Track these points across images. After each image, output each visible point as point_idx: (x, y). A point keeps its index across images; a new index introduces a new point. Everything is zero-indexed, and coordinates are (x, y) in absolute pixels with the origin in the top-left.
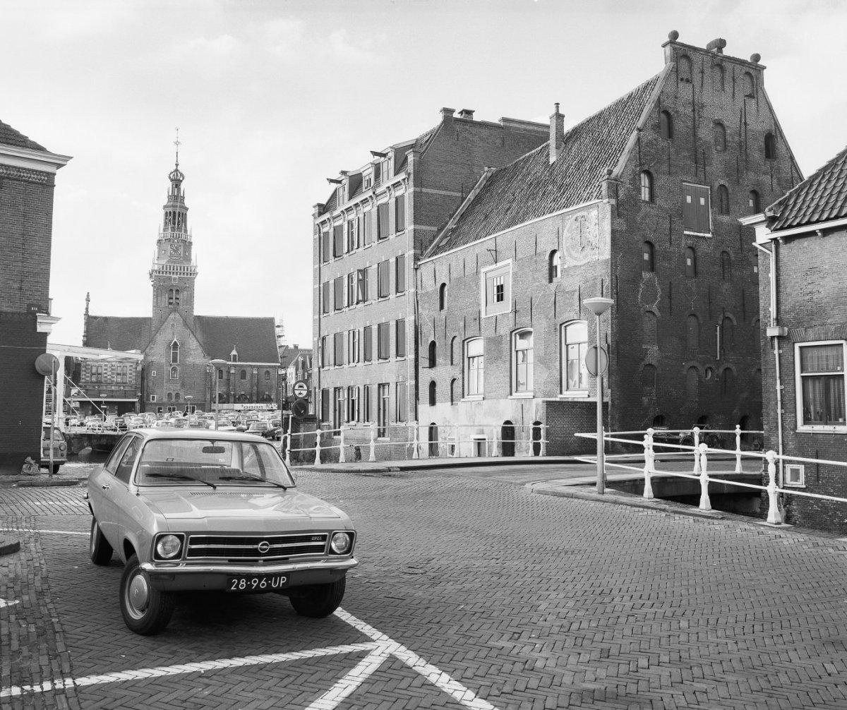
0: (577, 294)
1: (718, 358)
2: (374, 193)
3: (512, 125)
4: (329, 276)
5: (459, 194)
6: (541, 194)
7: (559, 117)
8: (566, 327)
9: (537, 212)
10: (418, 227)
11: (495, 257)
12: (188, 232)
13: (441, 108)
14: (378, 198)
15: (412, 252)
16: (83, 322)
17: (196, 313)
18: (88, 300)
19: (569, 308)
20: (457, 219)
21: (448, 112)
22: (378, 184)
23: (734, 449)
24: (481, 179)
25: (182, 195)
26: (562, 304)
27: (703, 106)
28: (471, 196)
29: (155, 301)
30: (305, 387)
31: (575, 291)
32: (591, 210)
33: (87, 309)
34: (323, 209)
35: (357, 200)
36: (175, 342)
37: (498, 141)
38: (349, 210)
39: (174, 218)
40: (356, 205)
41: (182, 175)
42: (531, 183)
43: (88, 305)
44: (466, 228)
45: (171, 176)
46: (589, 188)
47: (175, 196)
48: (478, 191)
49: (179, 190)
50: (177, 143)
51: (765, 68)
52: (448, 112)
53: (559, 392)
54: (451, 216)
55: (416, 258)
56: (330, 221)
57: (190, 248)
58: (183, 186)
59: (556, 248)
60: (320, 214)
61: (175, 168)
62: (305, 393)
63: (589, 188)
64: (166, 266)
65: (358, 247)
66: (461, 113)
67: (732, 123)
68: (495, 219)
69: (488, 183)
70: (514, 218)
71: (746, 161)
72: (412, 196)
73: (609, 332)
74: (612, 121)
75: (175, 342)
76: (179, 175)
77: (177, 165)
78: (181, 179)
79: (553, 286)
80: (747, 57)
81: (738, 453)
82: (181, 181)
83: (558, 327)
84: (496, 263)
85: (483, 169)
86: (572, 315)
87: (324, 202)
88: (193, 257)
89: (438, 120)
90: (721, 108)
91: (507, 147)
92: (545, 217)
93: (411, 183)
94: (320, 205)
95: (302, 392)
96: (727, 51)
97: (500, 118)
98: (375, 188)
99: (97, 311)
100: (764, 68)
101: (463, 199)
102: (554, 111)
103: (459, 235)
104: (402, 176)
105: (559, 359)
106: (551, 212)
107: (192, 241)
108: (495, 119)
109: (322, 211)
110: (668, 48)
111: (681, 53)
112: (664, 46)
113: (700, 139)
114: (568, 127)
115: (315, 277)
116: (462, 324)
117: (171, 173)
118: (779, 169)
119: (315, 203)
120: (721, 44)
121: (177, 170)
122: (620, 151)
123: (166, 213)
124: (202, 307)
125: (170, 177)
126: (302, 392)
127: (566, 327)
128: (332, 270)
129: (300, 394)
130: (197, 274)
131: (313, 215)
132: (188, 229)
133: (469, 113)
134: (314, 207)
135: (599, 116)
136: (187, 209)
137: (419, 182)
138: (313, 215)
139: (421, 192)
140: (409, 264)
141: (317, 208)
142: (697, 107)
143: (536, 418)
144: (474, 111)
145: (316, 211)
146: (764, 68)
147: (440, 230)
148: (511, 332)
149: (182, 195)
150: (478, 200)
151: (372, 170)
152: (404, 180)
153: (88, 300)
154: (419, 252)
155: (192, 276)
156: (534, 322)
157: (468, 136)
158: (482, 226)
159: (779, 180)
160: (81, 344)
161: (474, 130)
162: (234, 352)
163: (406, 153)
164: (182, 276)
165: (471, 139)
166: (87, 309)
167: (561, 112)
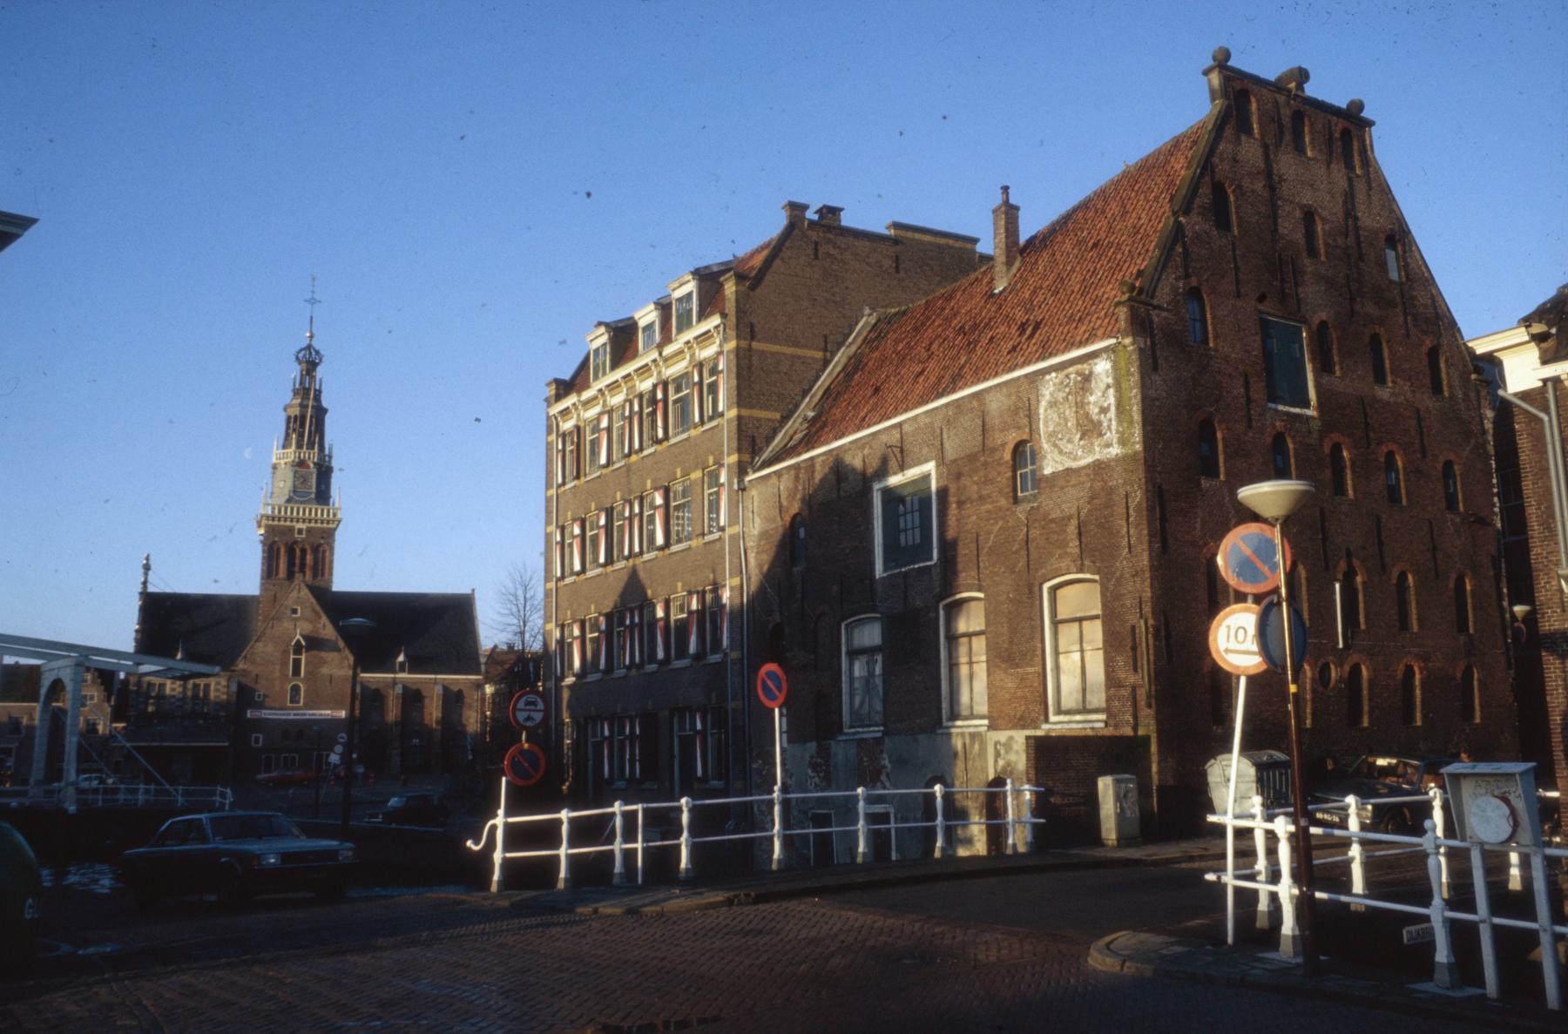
3: (910, 234)
5: (819, 355)
7: (1009, 213)
8: (1054, 589)
10: (746, 412)
11: (900, 459)
13: (785, 202)
16: (136, 603)
18: (147, 568)
20: (818, 397)
21: (796, 209)
23: (571, 845)
27: (1281, 179)
30: (541, 706)
31: (1070, 518)
32: (1096, 361)
35: (629, 368)
36: (298, 641)
37: (888, 263)
38: (613, 386)
40: (627, 377)
41: (317, 352)
43: (146, 574)
44: (837, 412)
45: (301, 355)
47: (304, 389)
48: (853, 348)
49: (313, 378)
50: (313, 301)
52: (796, 209)
53: (1042, 718)
54: (805, 393)
55: (741, 470)
56: (576, 409)
58: (320, 372)
59: (1025, 437)
60: (559, 397)
61: (308, 341)
62: (538, 717)
69: (873, 335)
75: (298, 641)
76: (313, 353)
80: (1342, 103)
81: (618, 846)
82: (317, 364)
89: (773, 225)
94: (558, 382)
96: (1311, 90)
97: (889, 221)
98: (660, 347)
99: (168, 582)
100: (1370, 124)
101: (826, 363)
102: (998, 199)
108: (879, 226)
112: (1206, 73)
114: (1028, 228)
119: (551, 378)
125: (297, 358)
126: (533, 714)
129: (529, 718)
130: (339, 521)
134: (548, 384)
135: (1084, 206)
139: (750, 349)
141: (554, 386)
144: (841, 210)
145: (552, 391)
147: (785, 419)
153: (147, 568)
154: (746, 457)
155: (331, 526)
157: (832, 251)
158: (868, 407)
161: (840, 241)
162: (401, 658)
164: (312, 525)
165: (839, 257)
166: (145, 583)
167: (1012, 201)
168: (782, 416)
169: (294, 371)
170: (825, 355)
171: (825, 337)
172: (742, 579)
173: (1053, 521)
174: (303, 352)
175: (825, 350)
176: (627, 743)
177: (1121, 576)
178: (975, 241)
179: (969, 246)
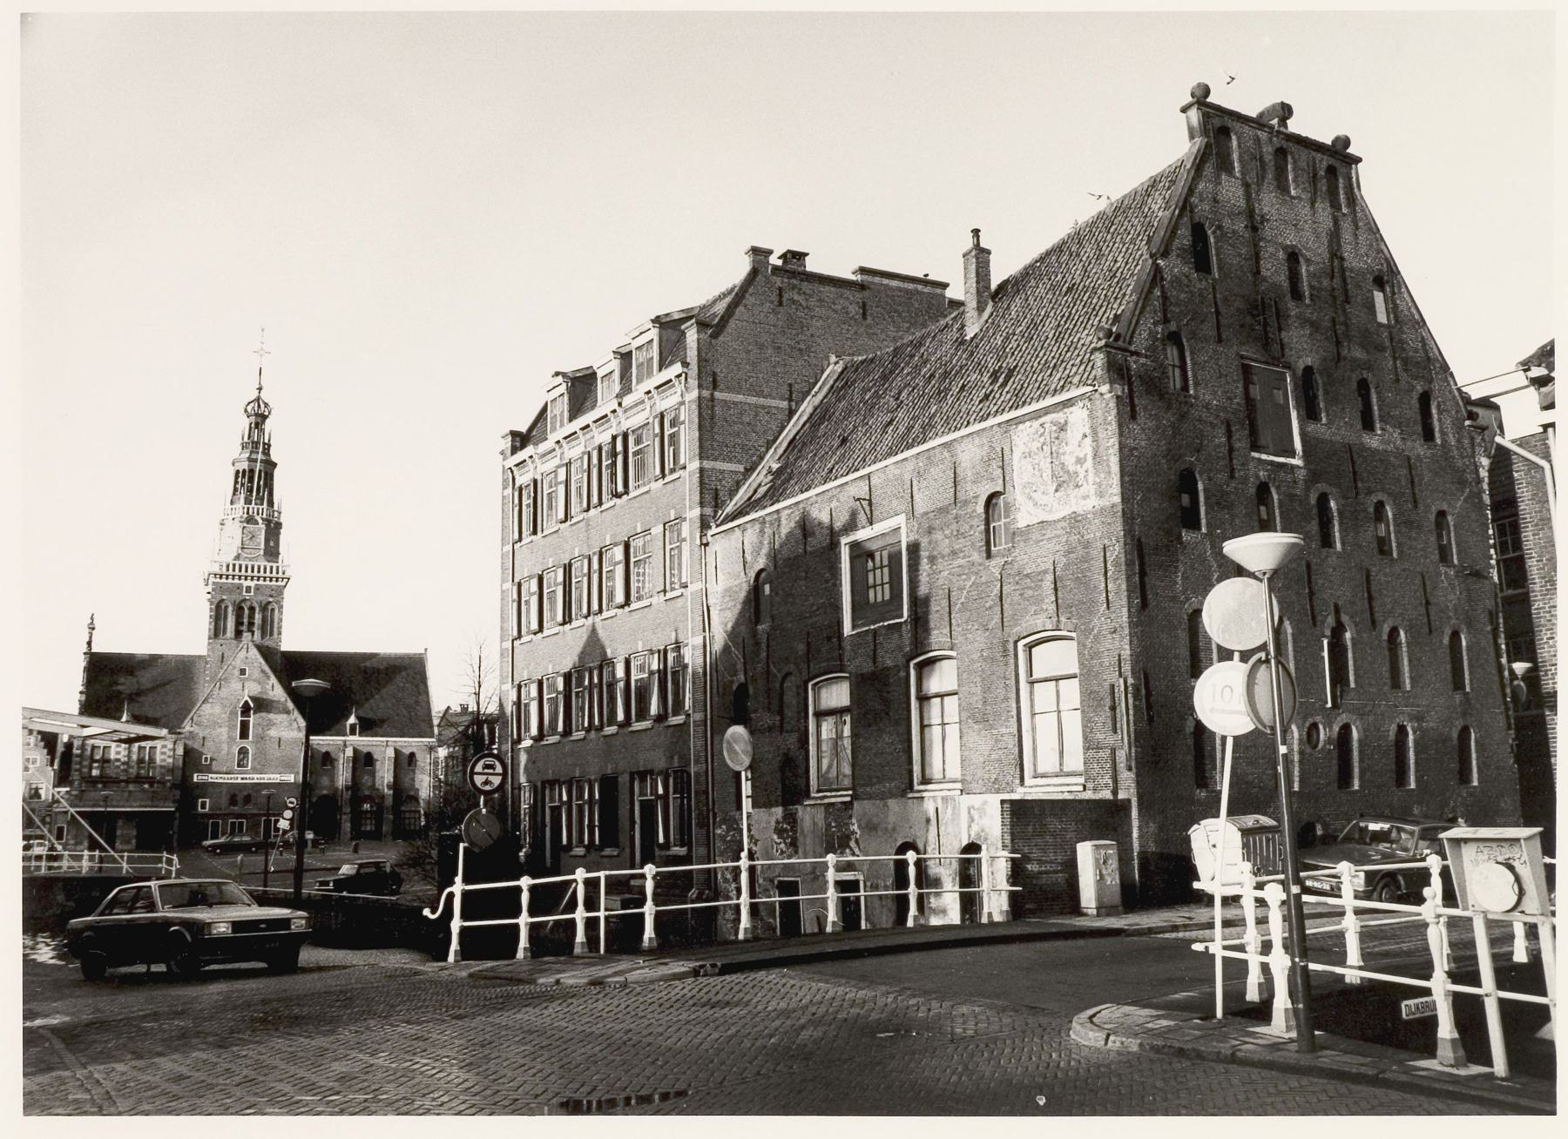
0: (1050, 577)
1: (1329, 705)
2: (620, 404)
4: (527, 567)
5: (784, 404)
6: (955, 390)
7: (980, 256)
9: (950, 425)
10: (708, 464)
12: (276, 508)
13: (749, 247)
14: (629, 413)
15: (697, 512)
16: (81, 663)
17: (283, 649)
19: (1034, 608)
21: (759, 254)
22: (626, 389)
24: (825, 376)
25: (266, 441)
26: (1017, 598)
27: (1263, 219)
28: (806, 408)
29: (212, 627)
30: (499, 769)
31: (1045, 572)
33: (89, 643)
34: (521, 440)
35: (587, 418)
39: (251, 480)
41: (266, 405)
42: (931, 375)
43: (91, 634)
45: (249, 408)
46: (1061, 369)
47: (253, 442)
51: (1358, 160)
52: (759, 254)
54: (769, 445)
55: (704, 525)
57: (279, 534)
58: (269, 425)
59: (999, 489)
60: (514, 450)
63: (1061, 369)
64: (234, 565)
65: (567, 619)
66: (783, 256)
67: (1315, 249)
68: (862, 442)
70: (903, 437)
71: (1346, 325)
72: (694, 407)
73: (1126, 653)
74: (1089, 250)
75: (246, 702)
76: (262, 406)
77: (260, 389)
78: (266, 413)
79: (995, 565)
82: (266, 417)
83: (1011, 647)
84: (871, 524)
85: (827, 358)
86: (1041, 621)
87: (523, 429)
88: (282, 549)
89: (743, 267)
90: (1295, 225)
91: (869, 320)
92: (971, 429)
93: (693, 382)
94: (514, 434)
95: (491, 778)
96: (1295, 126)
101: (791, 413)
102: (969, 243)
103: (791, 478)
104: (677, 368)
105: (1014, 713)
106: (983, 419)
107: (282, 520)
109: (518, 444)
110: (1194, 115)
111: (1217, 122)
112: (1184, 110)
113: (1265, 279)
115: (503, 569)
116: (802, 647)
117: (249, 403)
118: (1402, 342)
120: (1285, 111)
121: (258, 399)
122: (1116, 298)
123: (238, 472)
124: (295, 637)
125: (246, 411)
126: (491, 778)
127: (1030, 647)
128: (539, 555)
129: (486, 783)
131: (502, 453)
132: (275, 501)
133: (799, 256)
136: (275, 465)
137: (709, 378)
138: (502, 453)
140: (689, 530)
142: (1255, 223)
143: (970, 836)
145: (507, 443)
146: (1358, 160)
147: (749, 471)
148: (908, 661)
149: (266, 441)
150: (821, 415)
151: (615, 365)
152: (679, 376)
154: (709, 511)
155: (279, 583)
156: (958, 640)
159: (1405, 361)
160: (76, 712)
161: (805, 286)
163: (683, 327)
164: (261, 582)
165: (804, 303)
166: (89, 643)
168: (745, 469)
169: (245, 423)
170: (790, 406)
171: (790, 385)
172: (705, 637)
173: (1027, 576)
174: (252, 404)
175: (790, 400)
176: (586, 807)
177: (1100, 632)
178: (945, 286)
179: (939, 291)
